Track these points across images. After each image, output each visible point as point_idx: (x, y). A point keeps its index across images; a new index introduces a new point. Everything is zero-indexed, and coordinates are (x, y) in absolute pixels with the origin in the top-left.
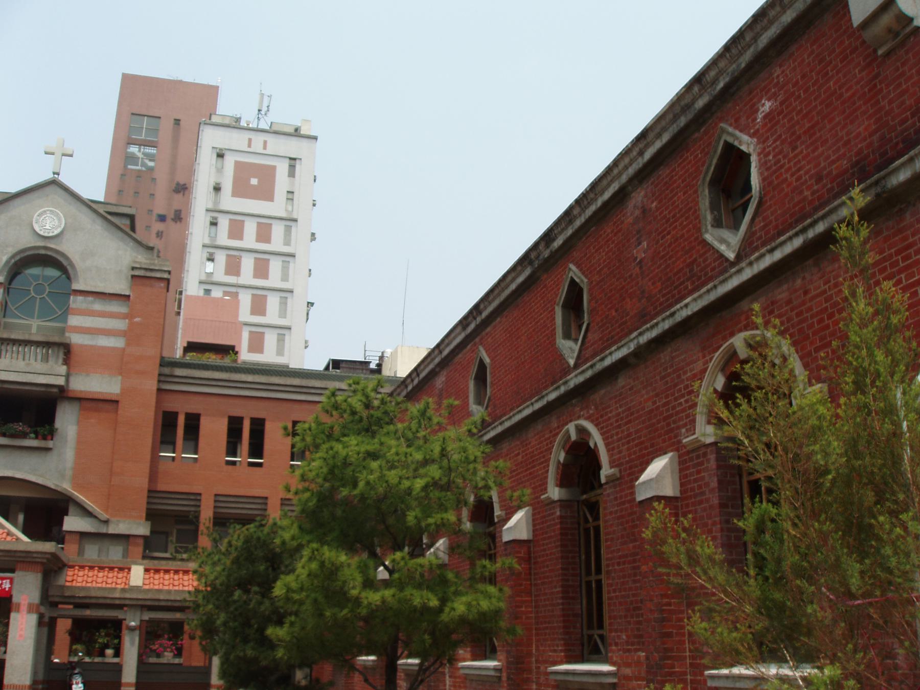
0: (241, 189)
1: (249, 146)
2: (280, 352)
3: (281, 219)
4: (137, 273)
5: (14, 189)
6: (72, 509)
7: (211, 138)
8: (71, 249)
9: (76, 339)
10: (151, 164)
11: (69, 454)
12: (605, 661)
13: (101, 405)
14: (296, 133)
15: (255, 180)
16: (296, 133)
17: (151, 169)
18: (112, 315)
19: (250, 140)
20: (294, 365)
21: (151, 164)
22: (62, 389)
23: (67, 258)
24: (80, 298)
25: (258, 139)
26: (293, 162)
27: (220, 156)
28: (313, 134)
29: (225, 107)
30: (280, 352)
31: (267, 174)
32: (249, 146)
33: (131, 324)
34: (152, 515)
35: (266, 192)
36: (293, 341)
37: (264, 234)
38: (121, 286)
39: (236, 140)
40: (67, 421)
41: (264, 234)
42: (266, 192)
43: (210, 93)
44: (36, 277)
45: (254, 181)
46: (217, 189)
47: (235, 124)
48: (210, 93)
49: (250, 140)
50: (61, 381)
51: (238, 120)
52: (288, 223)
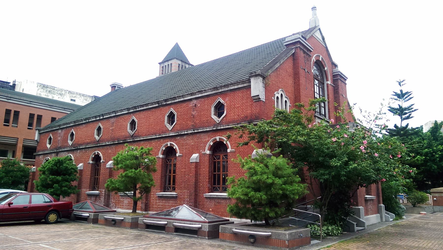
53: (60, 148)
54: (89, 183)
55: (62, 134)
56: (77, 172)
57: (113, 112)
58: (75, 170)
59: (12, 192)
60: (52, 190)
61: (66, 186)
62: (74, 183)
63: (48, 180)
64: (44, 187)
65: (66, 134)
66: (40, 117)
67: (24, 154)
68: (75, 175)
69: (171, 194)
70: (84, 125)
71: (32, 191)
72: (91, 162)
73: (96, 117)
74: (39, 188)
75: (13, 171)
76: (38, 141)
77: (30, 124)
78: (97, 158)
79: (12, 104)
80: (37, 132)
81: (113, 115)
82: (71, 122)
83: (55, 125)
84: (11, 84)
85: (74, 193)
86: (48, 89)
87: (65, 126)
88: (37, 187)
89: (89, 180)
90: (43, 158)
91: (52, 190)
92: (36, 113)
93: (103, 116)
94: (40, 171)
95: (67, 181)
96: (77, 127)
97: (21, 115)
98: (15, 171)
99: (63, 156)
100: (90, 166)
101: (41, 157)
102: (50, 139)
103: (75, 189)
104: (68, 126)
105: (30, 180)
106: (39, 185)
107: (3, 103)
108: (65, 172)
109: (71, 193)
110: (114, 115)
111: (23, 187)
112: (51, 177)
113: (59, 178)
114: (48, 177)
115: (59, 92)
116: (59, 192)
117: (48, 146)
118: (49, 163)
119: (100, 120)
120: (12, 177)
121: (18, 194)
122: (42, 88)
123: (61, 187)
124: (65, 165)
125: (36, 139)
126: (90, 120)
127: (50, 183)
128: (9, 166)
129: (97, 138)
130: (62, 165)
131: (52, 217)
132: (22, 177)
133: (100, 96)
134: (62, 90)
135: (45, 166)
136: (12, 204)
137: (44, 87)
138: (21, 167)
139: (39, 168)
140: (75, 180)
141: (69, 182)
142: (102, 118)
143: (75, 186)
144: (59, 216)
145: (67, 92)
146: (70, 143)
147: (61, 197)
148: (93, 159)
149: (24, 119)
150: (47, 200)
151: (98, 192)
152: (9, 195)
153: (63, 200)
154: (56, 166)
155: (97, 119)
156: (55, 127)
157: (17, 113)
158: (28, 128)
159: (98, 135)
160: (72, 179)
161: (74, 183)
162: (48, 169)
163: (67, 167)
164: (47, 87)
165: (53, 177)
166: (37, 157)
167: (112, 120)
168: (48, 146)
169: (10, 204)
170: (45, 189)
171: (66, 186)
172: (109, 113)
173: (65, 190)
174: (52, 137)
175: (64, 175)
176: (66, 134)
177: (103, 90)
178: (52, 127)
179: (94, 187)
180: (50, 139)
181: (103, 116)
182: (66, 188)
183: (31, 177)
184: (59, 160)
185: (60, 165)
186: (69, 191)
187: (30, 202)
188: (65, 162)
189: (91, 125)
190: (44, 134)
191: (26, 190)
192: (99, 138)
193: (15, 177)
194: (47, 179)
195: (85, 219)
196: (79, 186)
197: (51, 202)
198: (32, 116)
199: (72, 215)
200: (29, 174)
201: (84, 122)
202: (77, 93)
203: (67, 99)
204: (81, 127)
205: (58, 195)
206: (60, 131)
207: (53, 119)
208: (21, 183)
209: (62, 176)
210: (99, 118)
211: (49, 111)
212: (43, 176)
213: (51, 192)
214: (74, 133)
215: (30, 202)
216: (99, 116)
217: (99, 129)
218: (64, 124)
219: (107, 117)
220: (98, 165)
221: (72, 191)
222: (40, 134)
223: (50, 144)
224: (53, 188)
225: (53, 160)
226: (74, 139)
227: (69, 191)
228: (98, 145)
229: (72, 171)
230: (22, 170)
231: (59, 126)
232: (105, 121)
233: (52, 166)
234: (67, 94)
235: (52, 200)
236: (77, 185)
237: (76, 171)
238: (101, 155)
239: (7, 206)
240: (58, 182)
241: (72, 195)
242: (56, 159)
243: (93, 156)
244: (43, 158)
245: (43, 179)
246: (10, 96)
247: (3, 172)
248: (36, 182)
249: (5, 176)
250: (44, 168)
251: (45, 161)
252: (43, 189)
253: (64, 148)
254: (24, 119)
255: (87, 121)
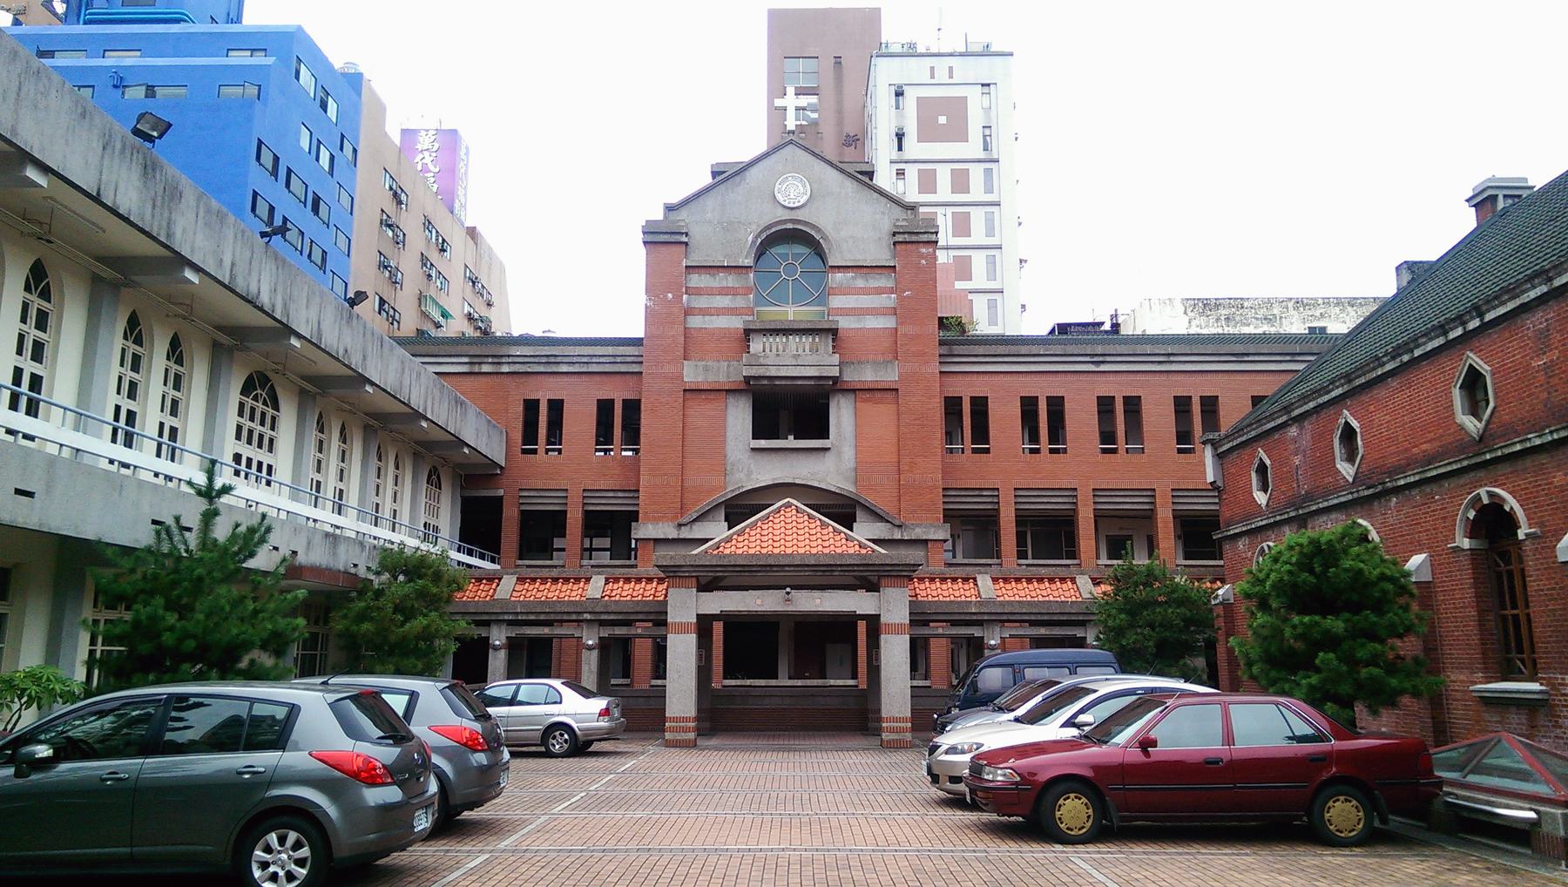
0: (928, 132)
1: (932, 77)
2: (993, 321)
3: (979, 161)
4: (900, 238)
5: (747, 158)
6: (859, 514)
7: (886, 73)
8: (823, 220)
9: (844, 323)
10: (815, 115)
11: (848, 454)
12: (1532, 678)
13: (878, 395)
14: (986, 52)
15: (945, 118)
16: (986, 52)
17: (815, 123)
18: (879, 291)
19: (932, 69)
20: (1011, 331)
21: (815, 115)
22: (835, 380)
23: (819, 230)
24: (839, 275)
25: (942, 65)
26: (986, 89)
27: (899, 94)
28: (1006, 50)
29: (892, 33)
30: (993, 321)
31: (957, 107)
32: (932, 77)
33: (901, 299)
34: (949, 516)
35: (958, 132)
36: (1008, 305)
37: (960, 182)
38: (883, 256)
39: (912, 71)
40: (842, 415)
41: (960, 182)
42: (958, 132)
43: (871, 18)
44: (785, 257)
45: (942, 120)
46: (900, 137)
47: (911, 52)
48: (871, 18)
49: (932, 69)
50: (835, 372)
51: (912, 46)
52: (988, 165)
53: (1309, 497)
54: (1475, 640)
55: (1306, 441)
56: (1412, 595)
57: (1530, 279)
58: (1400, 584)
59: (1153, 690)
60: (1314, 680)
61: (1373, 661)
62: (1408, 647)
63: (1288, 632)
64: (1277, 670)
65: (1322, 437)
66: (1210, 405)
67: (1185, 546)
68: (1406, 608)
69: (1518, 692)
70: (1393, 383)
71: (1235, 687)
72: (1466, 543)
73: (1443, 329)
74: (1255, 670)
75: (1150, 604)
76: (1219, 483)
77: (1184, 436)
78: (1493, 524)
79: (1111, 378)
80: (1208, 452)
81: (1532, 294)
82: (1332, 382)
83: (1271, 419)
84: (1107, 327)
85: (1416, 694)
86: (1223, 312)
87: (1312, 405)
88: (1250, 664)
89: (1473, 629)
90: (1252, 547)
91: (1314, 680)
92: (1196, 390)
93: (1481, 315)
94: (1248, 596)
95: (1372, 636)
96: (1365, 398)
97: (1147, 409)
98: (1160, 604)
99: (1328, 528)
100: (1465, 562)
101: (1241, 544)
102: (1262, 470)
103: (1417, 674)
104: (1321, 401)
105: (1221, 638)
106: (1254, 654)
107: (1083, 377)
108: (1355, 597)
109: (1402, 692)
110: (1544, 289)
111: (1200, 662)
112: (1296, 619)
113: (1335, 624)
114: (1286, 620)
115: (1262, 313)
116: (1345, 689)
117: (1261, 498)
118: (1276, 560)
119: (1468, 336)
120: (1152, 626)
121: (1170, 702)
122: (1202, 314)
123: (1354, 663)
124: (1347, 563)
125: (1210, 478)
126: (1417, 353)
127: (1299, 646)
128: (1136, 584)
129: (1472, 425)
130: (1337, 566)
131: (1343, 813)
132: (1187, 627)
133: (1433, 256)
134: (1269, 303)
135: (1262, 576)
136: (1154, 743)
137: (1206, 306)
138: (1176, 588)
139: (1243, 585)
140: (1409, 630)
141: (1382, 642)
142: (1474, 324)
143: (1416, 660)
144: (1370, 804)
145: (1290, 305)
146: (1347, 470)
147: (1360, 710)
148: (1473, 530)
149: (1158, 419)
150: (1303, 729)
151: (1535, 686)
152: (1147, 701)
153: (1377, 730)
154: (1311, 571)
155: (1452, 335)
156: (1271, 417)
157: (1133, 405)
158: (1180, 451)
159: (1475, 411)
160: (1392, 626)
161: (1408, 647)
162: (1279, 586)
163: (1360, 571)
164: (1217, 306)
165: (1307, 619)
166: (1226, 547)
167: (1536, 321)
168: (1261, 498)
169: (1146, 744)
170: (1283, 674)
171: (1373, 661)
172: (1512, 291)
173: (1371, 678)
174: (1268, 462)
175: (1356, 608)
176: (1322, 437)
177: (1444, 227)
178: (1259, 422)
179: (1509, 661)
180: (1262, 470)
181: (1481, 315)
182: (1375, 671)
183: (1220, 623)
184: (1314, 543)
185: (1326, 566)
186: (1394, 682)
187: (1229, 738)
188: (1345, 552)
189: (1428, 372)
190: (1235, 455)
191: (1213, 681)
192: (1480, 426)
193: (1161, 625)
194: (1282, 631)
195: (1519, 836)
196: (1431, 661)
197: (1318, 738)
198: (1182, 405)
199: (1437, 805)
200: (1211, 611)
201: (1388, 367)
202: (1327, 302)
203: (1295, 325)
204: (1380, 392)
205: (1347, 703)
206: (1293, 431)
207: (1256, 400)
208: (1188, 649)
209: (1347, 615)
210: (1459, 331)
211: (1239, 377)
212: (1261, 618)
213: (1312, 688)
214: (1355, 424)
215: (1229, 738)
216: (1460, 320)
217: (1473, 382)
218: (1304, 399)
219: (1502, 311)
220: (1505, 556)
221: (1407, 685)
222: (1220, 457)
223: (1264, 488)
224: (1318, 670)
225: (1291, 548)
226: (1361, 451)
227: (1394, 682)
228: (1481, 459)
229: (1384, 592)
230: (1182, 599)
231: (1287, 409)
232: (1494, 334)
233: (1290, 572)
234: (1292, 312)
235: (1324, 727)
236: (1419, 652)
237: (1403, 590)
238: (1511, 503)
239: (1136, 755)
240: (1330, 642)
241: (1406, 700)
242: (1304, 541)
243: (1472, 514)
244: (1252, 547)
245: (1265, 632)
246: (1099, 350)
247: (1121, 611)
248: (1241, 645)
249: (1131, 626)
250: (1261, 582)
251: (1264, 555)
252: (1273, 674)
253: (1325, 497)
254: (1158, 419)
255: (1406, 358)
